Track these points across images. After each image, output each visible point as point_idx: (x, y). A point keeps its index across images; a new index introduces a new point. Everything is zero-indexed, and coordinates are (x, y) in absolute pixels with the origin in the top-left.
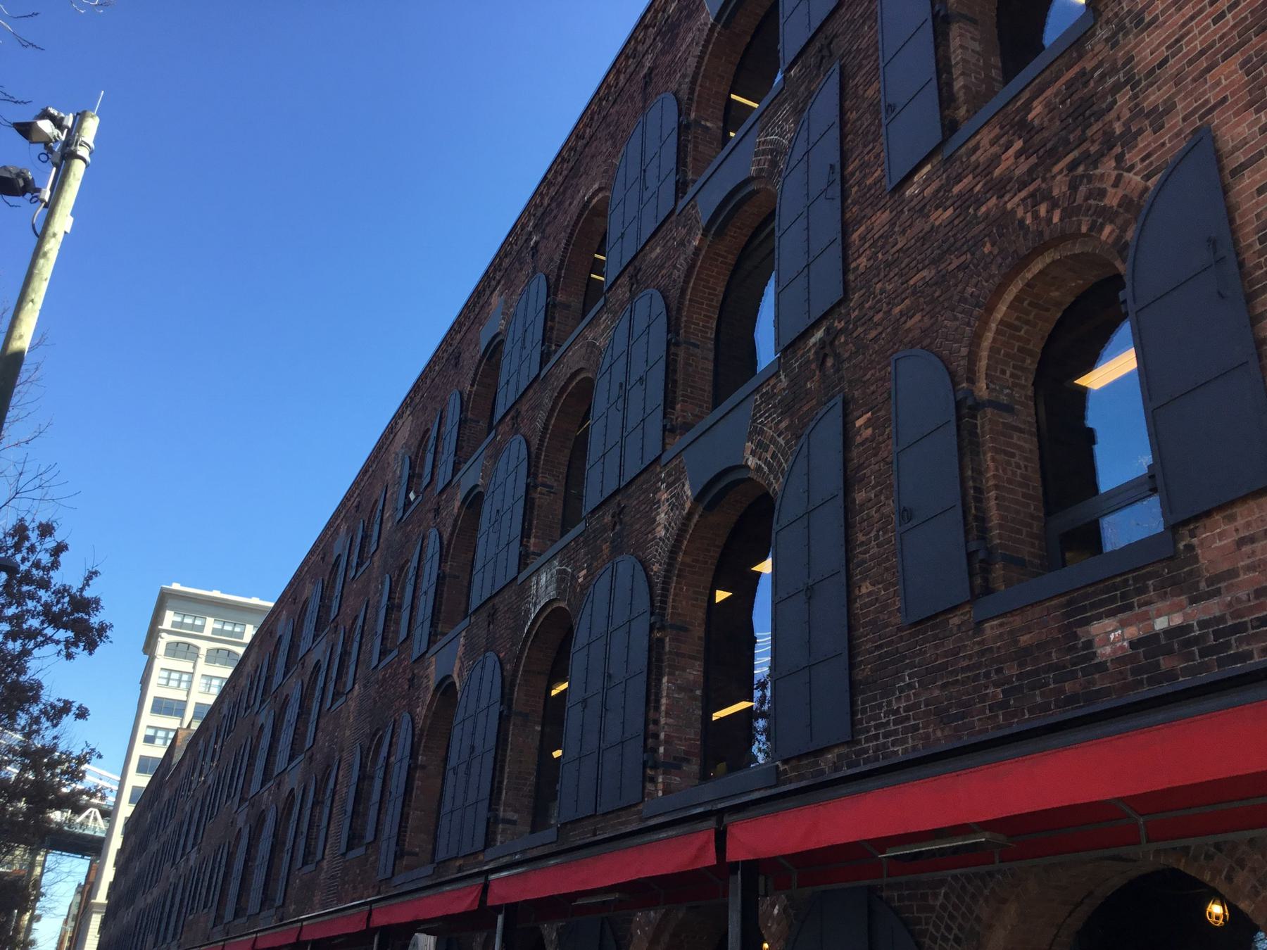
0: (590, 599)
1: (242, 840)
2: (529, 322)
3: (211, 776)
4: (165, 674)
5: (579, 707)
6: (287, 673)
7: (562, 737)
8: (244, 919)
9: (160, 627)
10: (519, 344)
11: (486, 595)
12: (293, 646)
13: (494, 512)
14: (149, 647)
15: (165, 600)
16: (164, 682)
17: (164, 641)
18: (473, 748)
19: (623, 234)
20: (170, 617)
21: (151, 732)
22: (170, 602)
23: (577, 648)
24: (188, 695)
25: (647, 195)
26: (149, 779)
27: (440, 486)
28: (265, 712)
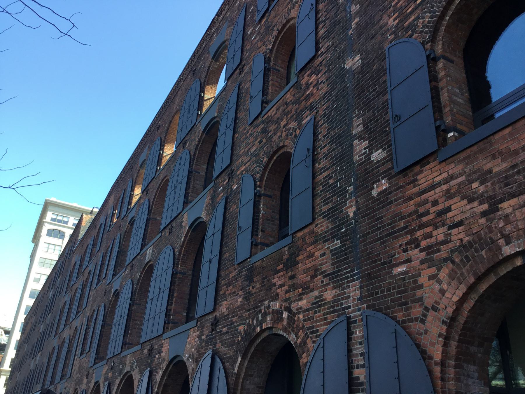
0: (215, 214)
1: (66, 343)
2: (191, 101)
3: (250, 61)
4: (47, 245)
5: (150, 301)
6: (78, 278)
7: (288, 217)
8: (65, 380)
9: (44, 220)
10: (151, 164)
11: (168, 222)
12: (81, 266)
13: (137, 228)
14: (36, 239)
15: (47, 206)
16: (46, 250)
17: (46, 228)
18: (160, 289)
19: (234, 55)
20: (50, 215)
21: (38, 276)
22: (50, 208)
23: (208, 237)
24: (62, 243)
25: (190, 115)
26: (34, 301)
27: (123, 216)
28: (67, 296)
